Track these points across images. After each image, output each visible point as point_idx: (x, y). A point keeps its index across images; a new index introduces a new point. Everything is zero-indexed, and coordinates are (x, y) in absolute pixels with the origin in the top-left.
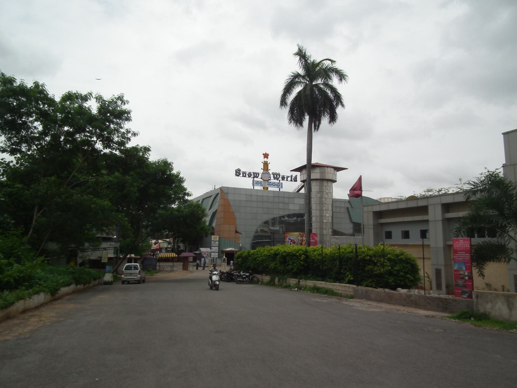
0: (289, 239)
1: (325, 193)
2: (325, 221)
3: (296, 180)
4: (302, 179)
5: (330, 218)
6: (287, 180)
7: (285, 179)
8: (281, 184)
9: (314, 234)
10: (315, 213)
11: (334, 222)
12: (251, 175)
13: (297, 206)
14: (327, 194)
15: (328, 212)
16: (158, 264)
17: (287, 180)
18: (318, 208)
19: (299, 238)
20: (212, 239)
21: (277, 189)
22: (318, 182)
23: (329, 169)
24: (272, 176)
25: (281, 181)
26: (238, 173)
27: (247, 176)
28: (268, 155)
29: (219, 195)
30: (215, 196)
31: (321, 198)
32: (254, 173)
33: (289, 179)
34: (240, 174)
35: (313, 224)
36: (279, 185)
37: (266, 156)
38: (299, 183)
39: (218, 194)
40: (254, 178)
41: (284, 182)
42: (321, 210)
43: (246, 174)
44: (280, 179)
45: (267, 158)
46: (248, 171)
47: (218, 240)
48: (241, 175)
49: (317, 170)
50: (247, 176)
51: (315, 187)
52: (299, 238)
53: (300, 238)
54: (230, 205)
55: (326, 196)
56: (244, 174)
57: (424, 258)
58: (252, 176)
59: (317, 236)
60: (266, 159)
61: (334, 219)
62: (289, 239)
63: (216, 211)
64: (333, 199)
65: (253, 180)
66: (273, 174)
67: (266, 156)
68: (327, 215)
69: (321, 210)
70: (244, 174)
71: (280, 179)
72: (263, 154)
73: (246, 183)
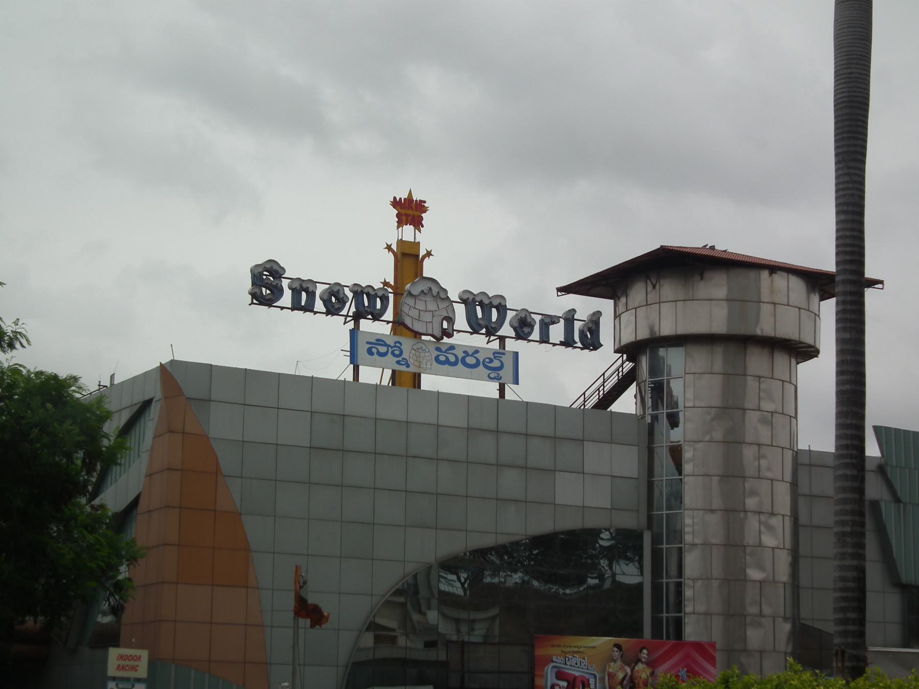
0: (560, 675)
1: (752, 417)
2: (754, 574)
3: (591, 341)
4: (628, 337)
5: (784, 559)
6: (545, 339)
7: (536, 335)
8: (508, 361)
9: (699, 647)
10: (698, 523)
11: (804, 581)
12: (342, 301)
13: (589, 494)
14: (768, 420)
15: (775, 522)
16: (144, 654)
17: (545, 339)
18: (717, 503)
19: (613, 667)
20: (112, 671)
21: (489, 390)
22: (719, 351)
23: (780, 280)
24: (460, 311)
25: (512, 345)
26: (267, 284)
27: (319, 305)
28: (421, 207)
29: (155, 411)
30: (125, 417)
31: (733, 443)
32: (358, 291)
33: (557, 332)
34: (277, 292)
35: (688, 593)
36: (501, 368)
37: (410, 211)
38: (604, 362)
39: (147, 404)
40: (357, 317)
41: (529, 352)
42: (733, 514)
43: (311, 295)
44: (506, 330)
45: (417, 223)
46: (324, 273)
47: (142, 672)
48: (287, 299)
49: (717, 287)
50: (319, 305)
51: (692, 381)
52: (613, 667)
53: (620, 671)
54: (217, 471)
55: (764, 434)
56: (304, 296)
57: (210, 661)
58: (350, 308)
59: (712, 660)
60: (408, 230)
61: (803, 564)
62: (560, 675)
63: (135, 503)
64: (797, 454)
65: (354, 333)
66: (469, 300)
67: (410, 211)
68: (769, 541)
69: (733, 514)
70: (304, 296)
71: (506, 330)
72: (396, 203)
73: (314, 347)
